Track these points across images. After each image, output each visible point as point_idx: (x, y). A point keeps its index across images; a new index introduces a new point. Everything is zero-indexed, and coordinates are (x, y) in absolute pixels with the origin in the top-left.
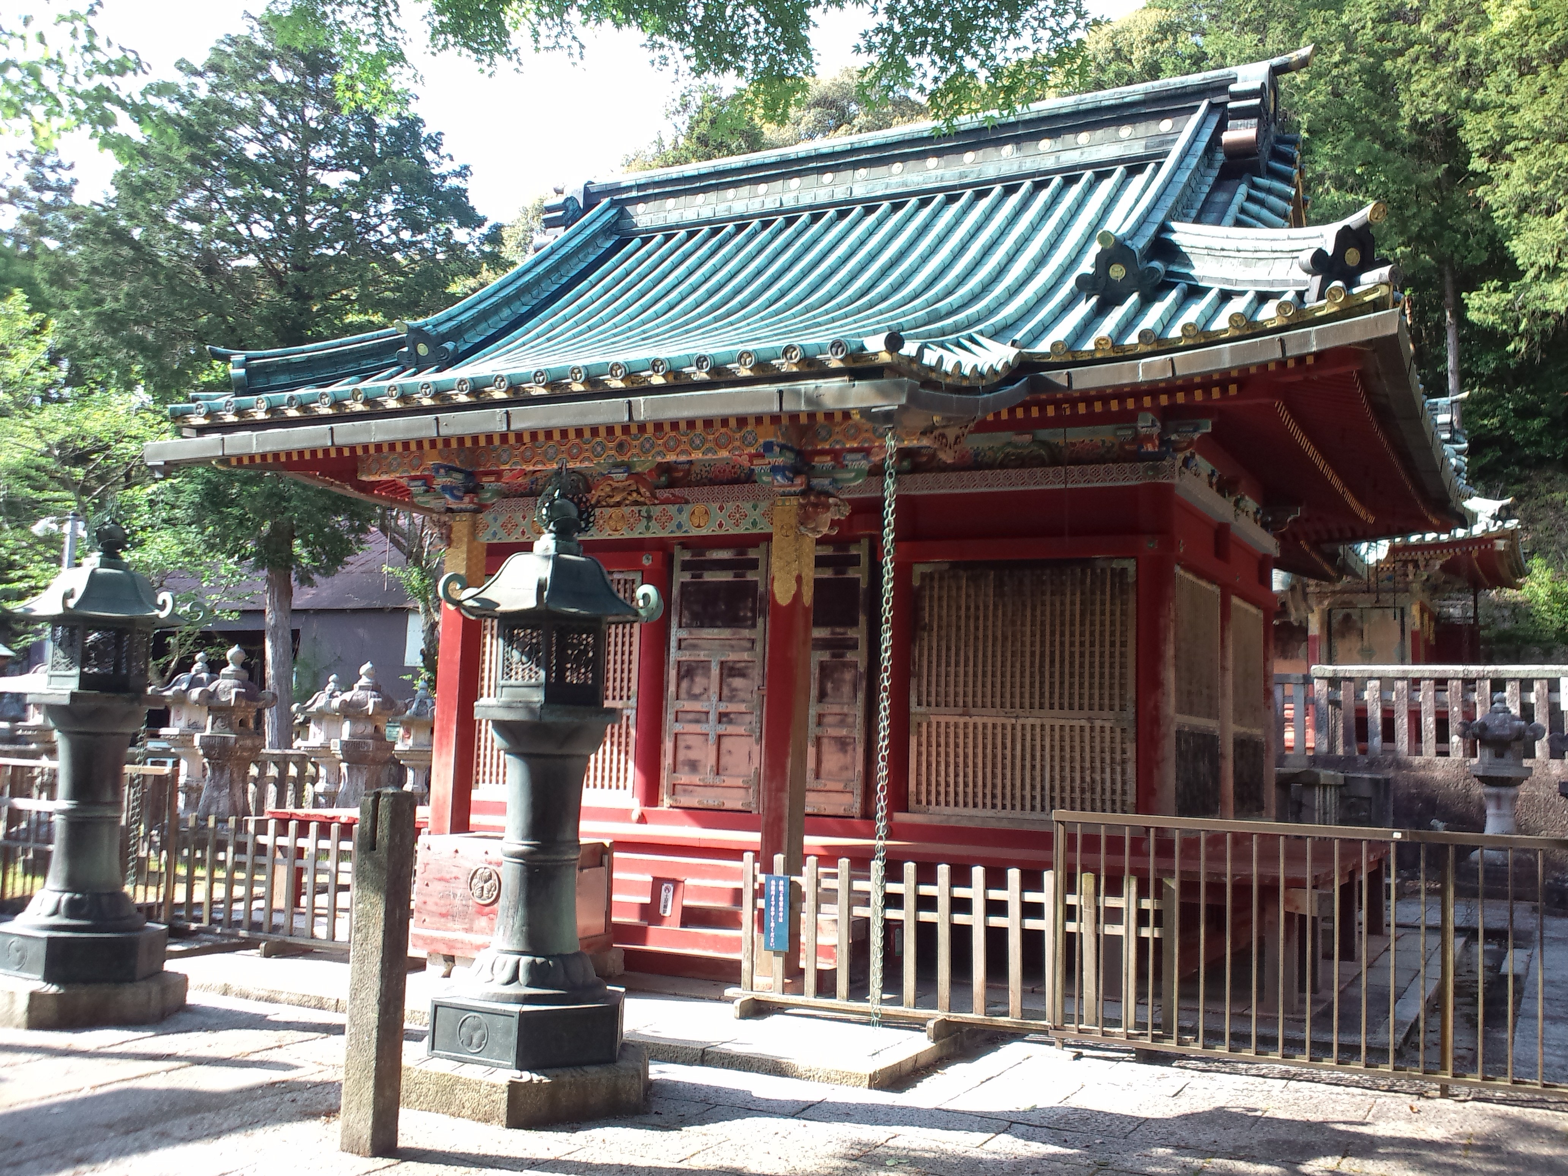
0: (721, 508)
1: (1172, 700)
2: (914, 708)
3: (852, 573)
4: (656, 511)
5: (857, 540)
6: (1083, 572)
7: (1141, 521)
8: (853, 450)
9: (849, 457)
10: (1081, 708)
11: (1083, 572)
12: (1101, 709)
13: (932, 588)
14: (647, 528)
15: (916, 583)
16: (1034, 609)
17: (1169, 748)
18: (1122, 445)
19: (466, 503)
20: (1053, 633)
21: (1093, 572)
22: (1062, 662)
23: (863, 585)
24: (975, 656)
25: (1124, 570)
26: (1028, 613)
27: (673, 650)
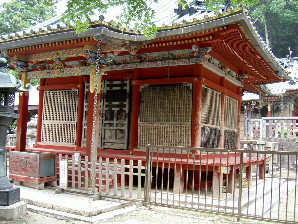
0: (79, 69)
1: (201, 118)
2: (139, 122)
3: (125, 88)
4: (65, 70)
5: (126, 80)
6: (180, 87)
7: (193, 73)
8: (109, 53)
9: (108, 54)
10: (178, 122)
11: (180, 87)
12: (183, 122)
13: (144, 92)
14: (63, 74)
15: (140, 90)
16: (168, 97)
17: (199, 132)
18: (190, 54)
19: (25, 70)
20: (172, 102)
21: (182, 87)
22: (174, 110)
23: (128, 91)
24: (154, 109)
25: (190, 86)
26: (167, 98)
27: (84, 108)
